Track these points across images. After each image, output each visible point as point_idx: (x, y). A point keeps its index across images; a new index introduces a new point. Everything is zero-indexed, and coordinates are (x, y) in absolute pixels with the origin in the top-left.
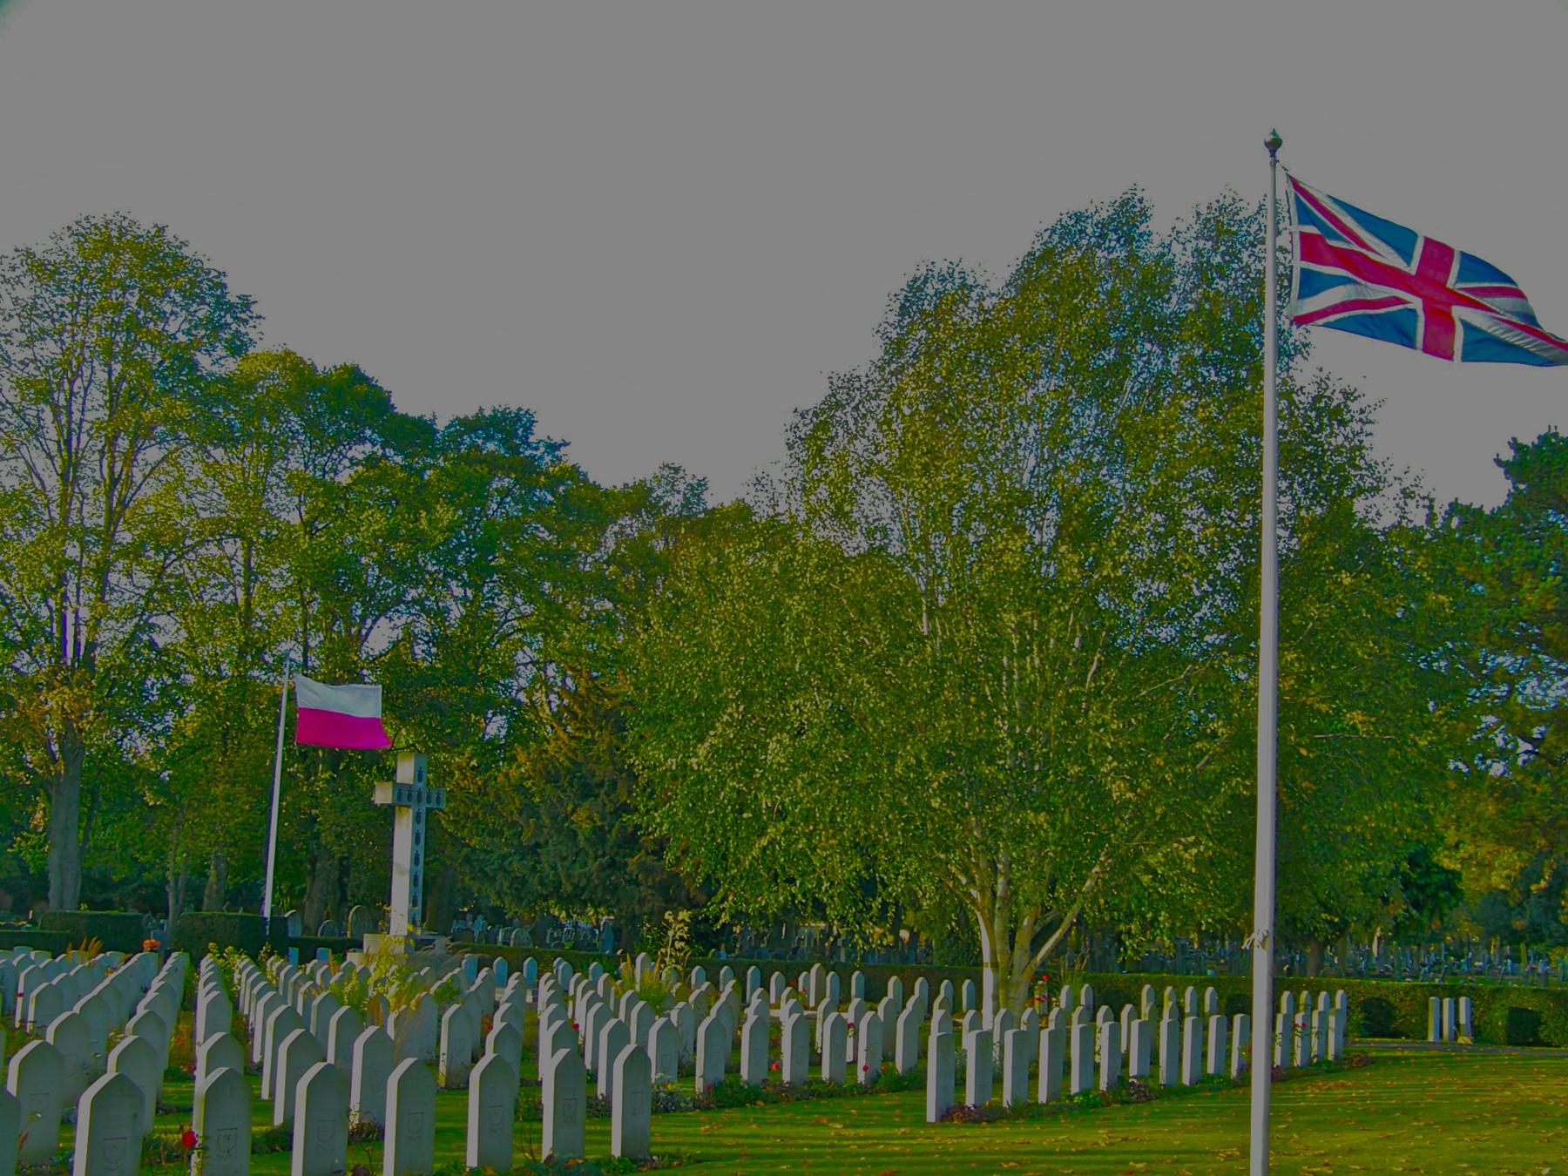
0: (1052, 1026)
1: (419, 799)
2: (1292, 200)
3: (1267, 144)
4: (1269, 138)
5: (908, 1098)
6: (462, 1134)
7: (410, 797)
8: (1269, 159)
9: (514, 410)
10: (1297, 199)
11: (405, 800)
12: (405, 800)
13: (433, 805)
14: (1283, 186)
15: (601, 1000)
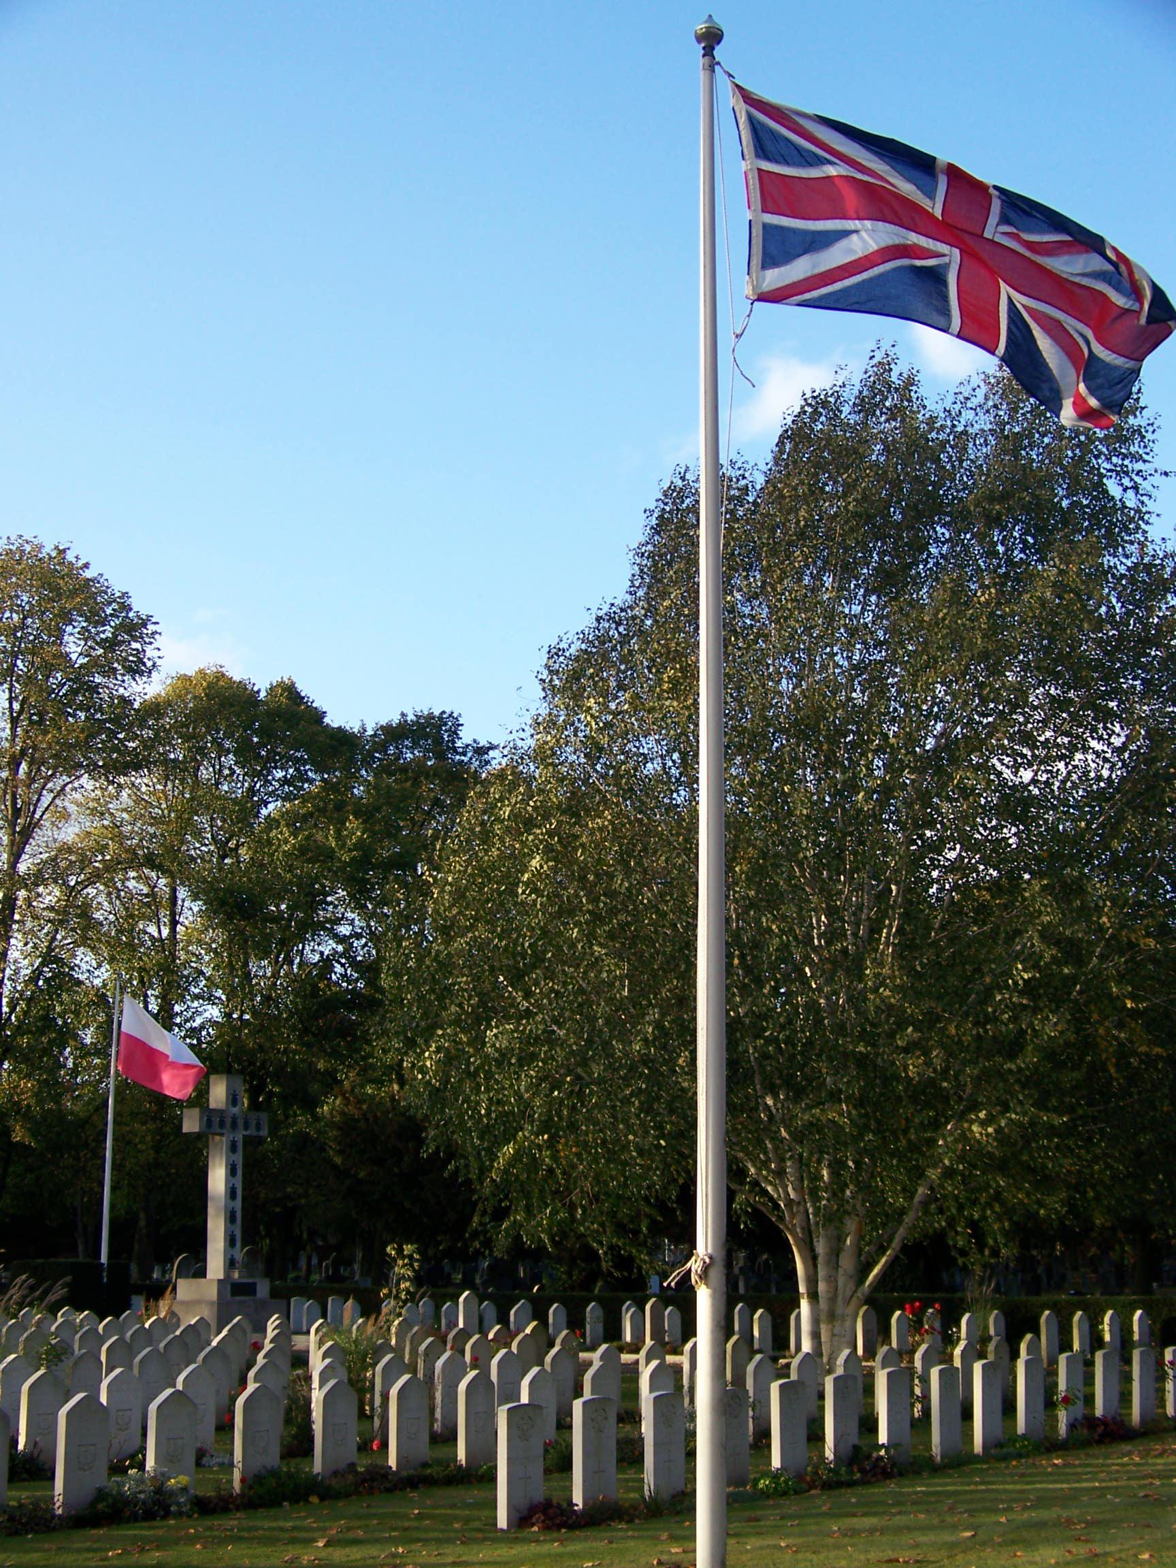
0: (587, 1394)
1: (234, 1125)
2: (743, 120)
3: (699, 39)
4: (701, 27)
5: (473, 1494)
6: (493, 1479)
7: (222, 1124)
8: (701, 61)
9: (437, 713)
10: (750, 118)
11: (216, 1128)
12: (216, 1128)
13: (252, 1132)
14: (728, 100)
15: (392, 1350)
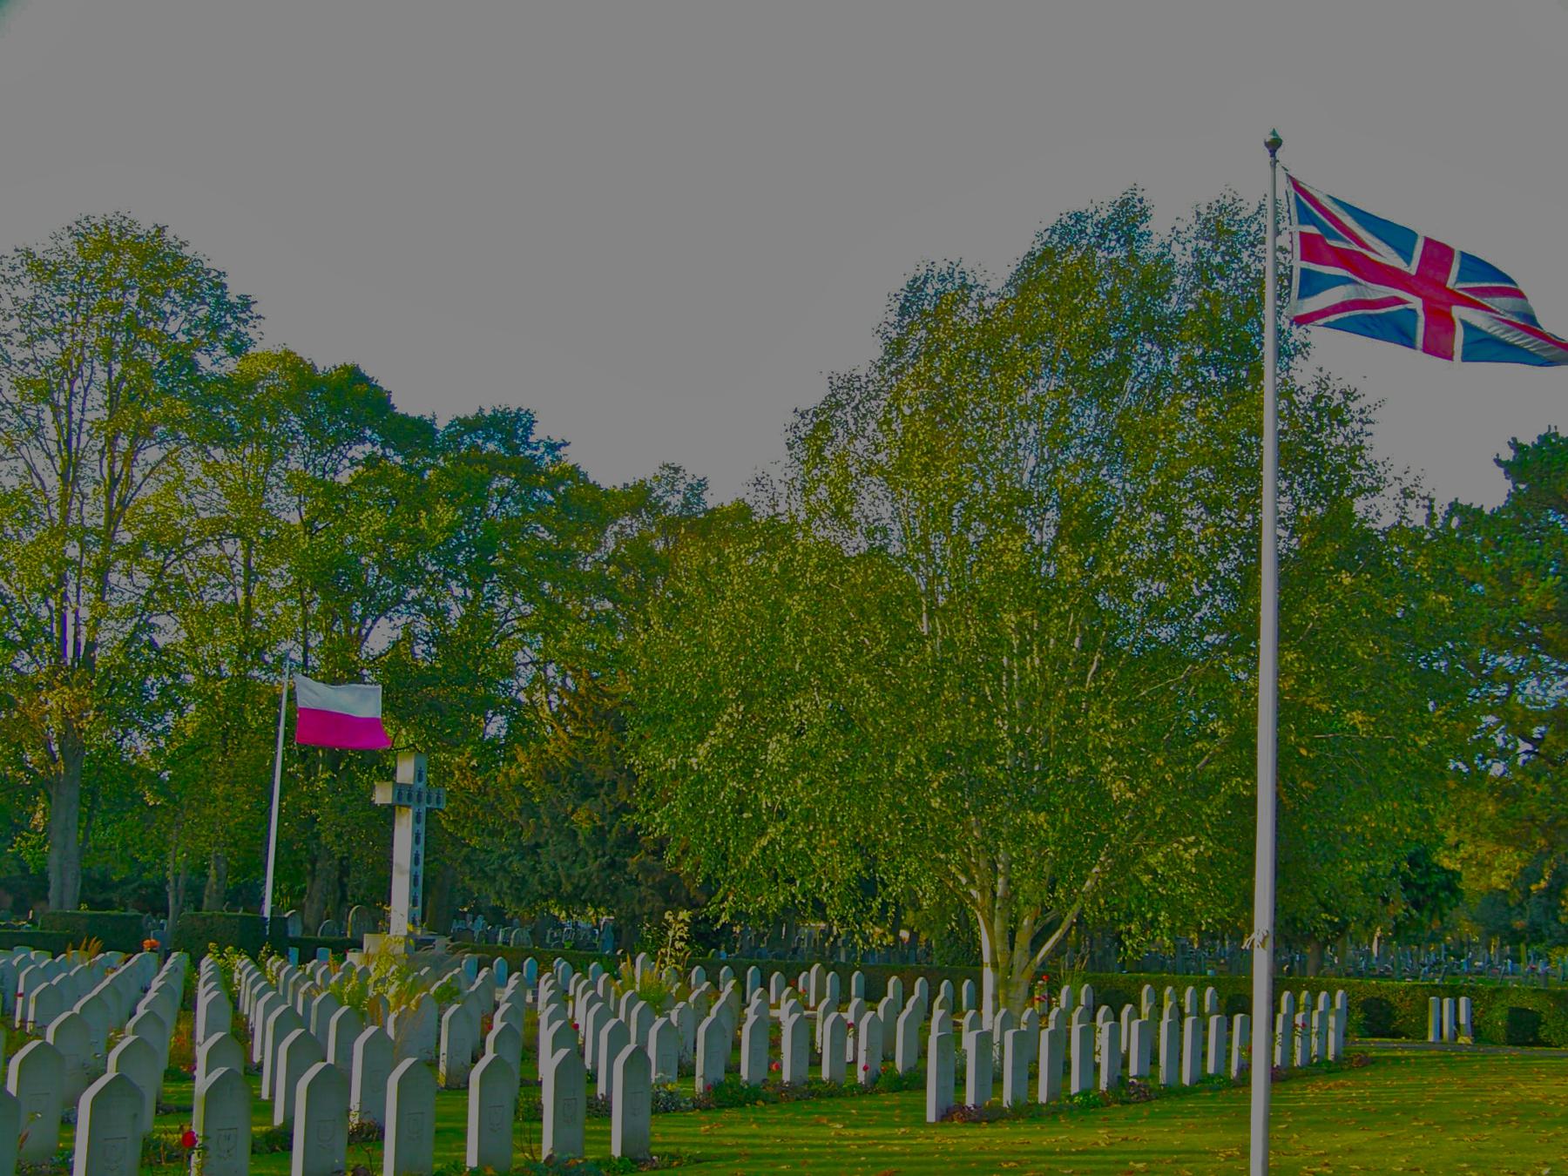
0: (1052, 1026)
1: (419, 799)
2: (1292, 200)
3: (1267, 144)
4: (1269, 138)
5: (908, 1098)
7: (410, 797)
8: (1269, 159)
9: (514, 410)
10: (1297, 199)
11: (405, 800)
12: (405, 800)
13: (433, 805)
14: (1283, 186)
15: (601, 1000)
